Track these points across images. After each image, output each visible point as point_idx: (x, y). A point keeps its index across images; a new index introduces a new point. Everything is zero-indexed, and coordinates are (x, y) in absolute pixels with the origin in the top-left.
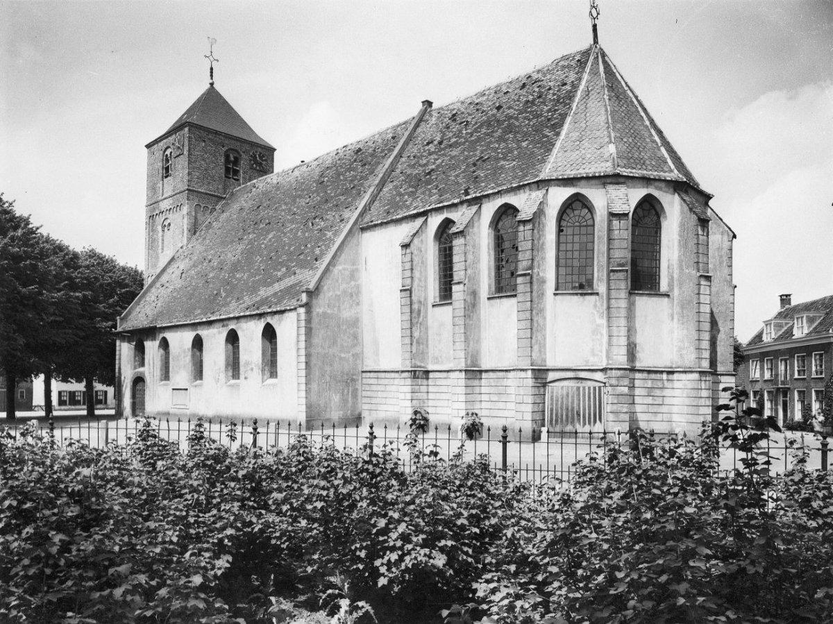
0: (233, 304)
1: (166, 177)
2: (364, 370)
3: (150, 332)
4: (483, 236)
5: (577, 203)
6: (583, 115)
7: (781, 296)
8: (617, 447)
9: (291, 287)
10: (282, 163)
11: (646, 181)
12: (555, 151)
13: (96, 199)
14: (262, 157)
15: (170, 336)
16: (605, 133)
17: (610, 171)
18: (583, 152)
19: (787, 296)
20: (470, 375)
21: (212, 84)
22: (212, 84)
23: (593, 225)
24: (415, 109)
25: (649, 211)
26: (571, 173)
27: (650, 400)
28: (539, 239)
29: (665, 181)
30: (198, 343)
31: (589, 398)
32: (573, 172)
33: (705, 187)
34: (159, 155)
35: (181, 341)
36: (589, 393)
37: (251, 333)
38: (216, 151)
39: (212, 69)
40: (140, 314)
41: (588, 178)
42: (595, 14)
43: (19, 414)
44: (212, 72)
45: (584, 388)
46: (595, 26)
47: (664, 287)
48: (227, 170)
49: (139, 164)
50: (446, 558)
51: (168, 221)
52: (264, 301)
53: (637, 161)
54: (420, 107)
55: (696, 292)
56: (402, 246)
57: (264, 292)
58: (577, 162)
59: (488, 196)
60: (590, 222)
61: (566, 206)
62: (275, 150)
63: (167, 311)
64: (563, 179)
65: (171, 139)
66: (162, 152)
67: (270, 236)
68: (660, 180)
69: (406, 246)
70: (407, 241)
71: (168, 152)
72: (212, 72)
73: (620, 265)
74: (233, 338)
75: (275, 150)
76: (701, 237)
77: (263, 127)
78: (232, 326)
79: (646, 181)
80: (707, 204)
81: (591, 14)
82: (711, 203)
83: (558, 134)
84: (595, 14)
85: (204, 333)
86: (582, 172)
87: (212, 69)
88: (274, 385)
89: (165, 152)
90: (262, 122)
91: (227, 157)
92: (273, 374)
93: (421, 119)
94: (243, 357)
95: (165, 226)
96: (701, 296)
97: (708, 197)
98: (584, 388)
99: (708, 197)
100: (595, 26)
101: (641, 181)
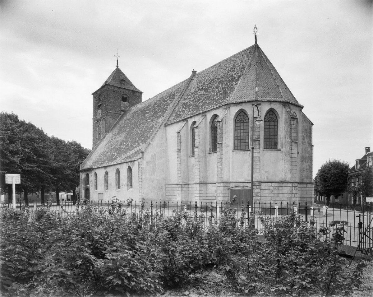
0: (118, 159)
2: (167, 184)
3: (90, 170)
5: (242, 112)
6: (247, 75)
7: (366, 148)
9: (138, 151)
10: (144, 98)
11: (270, 102)
12: (234, 91)
15: (97, 171)
16: (255, 83)
17: (254, 99)
18: (245, 91)
19: (368, 148)
20: (201, 185)
21: (117, 66)
22: (117, 66)
23: (249, 122)
24: (188, 75)
25: (272, 116)
26: (239, 101)
27: (272, 195)
29: (278, 102)
30: (107, 174)
32: (235, 101)
33: (301, 103)
35: (101, 173)
37: (112, 172)
39: (117, 61)
40: (88, 163)
41: (245, 102)
43: (30, 204)
44: (117, 62)
46: (256, 36)
47: (279, 147)
52: (129, 157)
53: (267, 94)
54: (191, 73)
55: (290, 149)
56: (177, 133)
57: (129, 153)
58: (243, 96)
59: (208, 111)
60: (247, 121)
61: (238, 114)
63: (95, 163)
64: (236, 103)
67: (134, 130)
68: (276, 102)
69: (178, 133)
70: (179, 131)
72: (117, 62)
73: (256, 139)
74: (118, 172)
75: (143, 93)
76: (292, 125)
77: (138, 84)
78: (118, 167)
79: (270, 102)
80: (301, 110)
82: (303, 111)
83: (237, 84)
85: (108, 169)
86: (244, 100)
87: (117, 61)
88: (132, 191)
90: (137, 82)
92: (131, 187)
93: (191, 79)
94: (121, 181)
96: (293, 151)
97: (302, 107)
99: (302, 107)
100: (256, 36)
101: (268, 102)
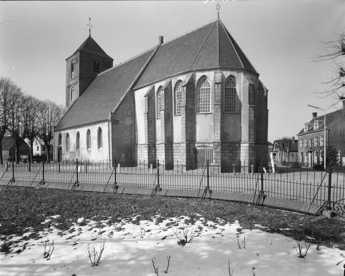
1: (72, 72)
4: (182, 90)
8: (210, 75)
10: (115, 64)
13: (49, 85)
14: (108, 62)
21: (90, 35)
22: (90, 35)
28: (204, 140)
31: (208, 153)
34: (70, 64)
36: (208, 152)
38: (91, 62)
39: (90, 29)
42: (218, 8)
44: (90, 31)
45: (206, 150)
48: (95, 68)
49: (63, 68)
50: (334, 173)
51: (73, 88)
62: (113, 60)
65: (74, 57)
66: (71, 62)
71: (73, 62)
72: (90, 31)
75: (113, 60)
77: (109, 53)
81: (217, 8)
84: (218, 8)
87: (90, 29)
89: (72, 62)
90: (108, 49)
91: (95, 63)
95: (72, 90)
98: (206, 150)
